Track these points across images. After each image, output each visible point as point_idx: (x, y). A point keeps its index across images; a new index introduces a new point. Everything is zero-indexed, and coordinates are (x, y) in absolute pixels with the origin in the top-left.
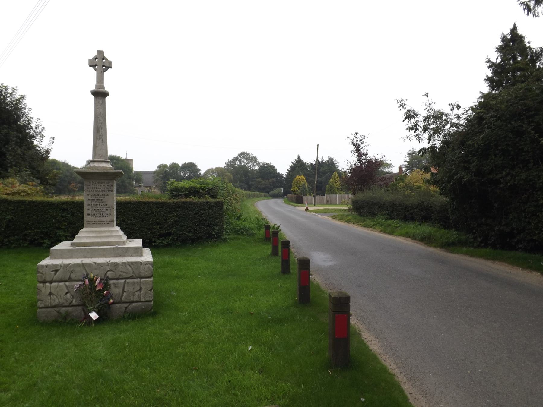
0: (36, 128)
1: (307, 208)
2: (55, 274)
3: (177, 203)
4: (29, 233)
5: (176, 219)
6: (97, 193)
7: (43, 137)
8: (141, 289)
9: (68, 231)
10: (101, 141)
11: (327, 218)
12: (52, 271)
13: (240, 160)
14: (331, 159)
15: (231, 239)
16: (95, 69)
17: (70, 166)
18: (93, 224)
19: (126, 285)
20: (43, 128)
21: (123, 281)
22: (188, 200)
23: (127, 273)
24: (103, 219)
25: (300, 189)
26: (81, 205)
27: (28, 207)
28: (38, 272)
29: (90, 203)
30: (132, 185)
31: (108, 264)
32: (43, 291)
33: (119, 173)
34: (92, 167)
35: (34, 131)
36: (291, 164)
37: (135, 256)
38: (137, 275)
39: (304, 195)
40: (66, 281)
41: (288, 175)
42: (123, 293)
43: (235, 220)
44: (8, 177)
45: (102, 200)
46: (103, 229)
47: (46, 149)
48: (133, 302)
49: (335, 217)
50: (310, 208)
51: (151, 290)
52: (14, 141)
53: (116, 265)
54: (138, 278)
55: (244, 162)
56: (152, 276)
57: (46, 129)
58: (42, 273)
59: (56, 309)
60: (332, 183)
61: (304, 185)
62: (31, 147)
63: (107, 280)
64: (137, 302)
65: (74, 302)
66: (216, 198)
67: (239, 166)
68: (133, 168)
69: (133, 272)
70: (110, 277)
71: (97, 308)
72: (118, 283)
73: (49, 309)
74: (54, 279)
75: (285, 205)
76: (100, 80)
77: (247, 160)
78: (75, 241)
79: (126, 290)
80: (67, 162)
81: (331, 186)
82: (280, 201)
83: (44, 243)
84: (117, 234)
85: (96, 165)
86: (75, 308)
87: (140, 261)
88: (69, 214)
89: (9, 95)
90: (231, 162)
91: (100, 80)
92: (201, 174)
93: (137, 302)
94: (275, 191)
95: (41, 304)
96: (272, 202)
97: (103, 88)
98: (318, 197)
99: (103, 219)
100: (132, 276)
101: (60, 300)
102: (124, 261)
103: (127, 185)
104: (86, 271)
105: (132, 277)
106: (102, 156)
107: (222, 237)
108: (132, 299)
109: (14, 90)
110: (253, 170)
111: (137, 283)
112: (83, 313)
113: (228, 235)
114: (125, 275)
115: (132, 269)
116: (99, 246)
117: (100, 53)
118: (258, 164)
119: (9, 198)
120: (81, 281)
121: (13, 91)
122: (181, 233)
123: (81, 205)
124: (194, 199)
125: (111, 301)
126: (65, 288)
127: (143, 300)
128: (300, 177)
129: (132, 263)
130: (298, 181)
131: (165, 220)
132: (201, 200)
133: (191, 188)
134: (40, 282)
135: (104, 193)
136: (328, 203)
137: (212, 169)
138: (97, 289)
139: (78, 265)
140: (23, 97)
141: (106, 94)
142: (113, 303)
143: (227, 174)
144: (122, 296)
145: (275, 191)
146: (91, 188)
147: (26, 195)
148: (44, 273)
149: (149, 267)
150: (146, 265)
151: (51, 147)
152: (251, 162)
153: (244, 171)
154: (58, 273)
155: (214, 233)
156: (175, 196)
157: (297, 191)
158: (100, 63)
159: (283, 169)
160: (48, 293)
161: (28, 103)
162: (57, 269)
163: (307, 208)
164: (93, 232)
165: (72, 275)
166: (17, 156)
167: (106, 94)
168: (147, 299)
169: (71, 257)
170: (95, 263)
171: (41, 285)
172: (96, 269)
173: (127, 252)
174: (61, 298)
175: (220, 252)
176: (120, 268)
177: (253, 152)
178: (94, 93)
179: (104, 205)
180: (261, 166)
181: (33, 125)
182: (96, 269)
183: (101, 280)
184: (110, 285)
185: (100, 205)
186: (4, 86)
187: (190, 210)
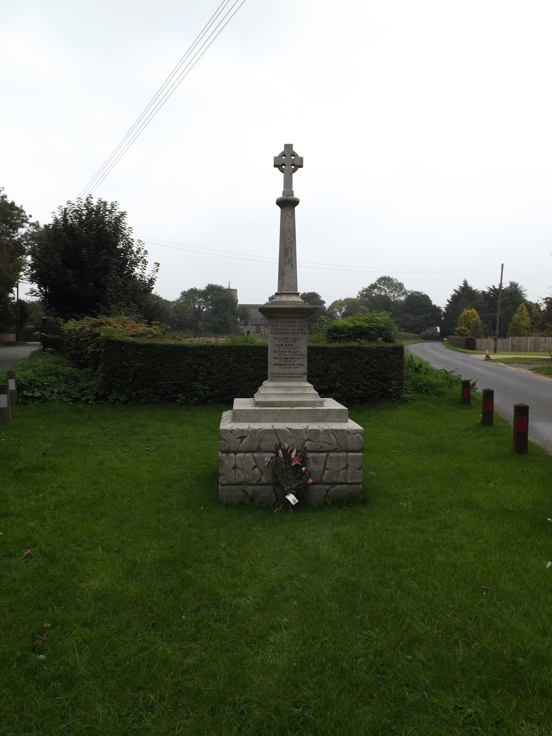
0: (137, 252)
1: (487, 356)
2: (241, 442)
3: (342, 348)
4: (161, 385)
5: (340, 370)
6: (286, 336)
7: (145, 262)
8: (346, 467)
9: (206, 383)
10: (290, 266)
11: (523, 371)
12: (238, 438)
13: (380, 289)
14: (514, 286)
15: (412, 399)
16: (282, 171)
17: (161, 298)
18: (279, 377)
19: (328, 460)
20: (146, 251)
21: (325, 454)
22: (355, 344)
23: (330, 444)
24: (294, 371)
25: (469, 328)
26: (263, 350)
27: (160, 352)
28: (221, 439)
29: (277, 349)
30: (237, 323)
31: (306, 431)
33: (310, 309)
34: (280, 302)
35: (135, 256)
36: (453, 293)
37: (338, 422)
38: (343, 448)
39: (477, 338)
40: (253, 452)
41: (448, 308)
42: (324, 471)
43: (413, 373)
44: (109, 315)
45: (292, 345)
46: (293, 384)
47: (150, 277)
48: (334, 484)
49: (537, 371)
50: (492, 357)
51: (360, 469)
52: (114, 269)
53: (316, 432)
54: (343, 451)
55: (386, 291)
56: (362, 449)
57: (149, 252)
58: (225, 440)
59: (240, 487)
60: (519, 321)
61: (477, 322)
62: (131, 278)
63: (304, 453)
64: (341, 483)
65: (263, 480)
66: (390, 341)
67: (379, 295)
68: (237, 301)
69: (338, 444)
70: (308, 448)
71: (295, 489)
72: (318, 457)
73: (233, 487)
74: (240, 449)
75: (447, 351)
76: (288, 183)
77: (389, 288)
78: (258, 398)
79: (328, 467)
80: (157, 294)
81: (516, 325)
82: (438, 345)
83: (178, 398)
84: (307, 392)
85: (284, 298)
86: (264, 487)
87: (346, 428)
88: (208, 362)
89: (107, 213)
90: (366, 290)
91: (288, 183)
92: (325, 308)
93: (341, 483)
94: (429, 331)
95: (223, 479)
96: (427, 346)
97: (292, 193)
98: (499, 341)
99: (294, 371)
100: (336, 449)
101: (247, 476)
102: (327, 428)
103: (231, 323)
104: (279, 440)
105: (335, 451)
106: (291, 287)
107: (401, 396)
108: (335, 480)
109: (113, 206)
110: (397, 301)
111: (343, 458)
112: (274, 495)
113: (408, 393)
115: (337, 439)
116: (286, 407)
117: (289, 147)
118: (405, 293)
119: (137, 340)
120: (273, 452)
121: (113, 207)
122: (347, 389)
123: (263, 350)
124: (365, 343)
125: (310, 481)
126: (252, 460)
127: (349, 481)
128: (469, 311)
129: (337, 431)
130: (466, 317)
131: (327, 371)
132: (373, 345)
133: (356, 328)
134: (223, 452)
135: (295, 336)
136: (514, 348)
137: (341, 300)
138: (293, 465)
139: (269, 431)
140: (123, 214)
141: (296, 202)
142: (312, 484)
143: (361, 307)
144: (323, 474)
145: (429, 331)
146: (278, 329)
147: (152, 337)
148: (228, 440)
149: (358, 437)
150: (354, 434)
151: (156, 275)
152: (395, 290)
153: (383, 303)
154: (244, 441)
155: (390, 390)
156: (335, 339)
157: (465, 331)
158: (288, 162)
159: (441, 300)
160: (232, 466)
161: (128, 222)
162: (244, 435)
163: (487, 356)
164: (281, 387)
165: (261, 444)
166: (119, 288)
167: (296, 202)
168: (355, 481)
169: (258, 421)
170: (290, 429)
171: (224, 455)
172: (291, 437)
173: (327, 415)
174: (248, 474)
175: (402, 415)
177: (398, 277)
178: (280, 203)
179: (294, 352)
180: (409, 296)
181: (135, 249)
182: (291, 437)
183: (297, 452)
184: (308, 459)
185: (289, 352)
186: (102, 202)
187: (359, 359)
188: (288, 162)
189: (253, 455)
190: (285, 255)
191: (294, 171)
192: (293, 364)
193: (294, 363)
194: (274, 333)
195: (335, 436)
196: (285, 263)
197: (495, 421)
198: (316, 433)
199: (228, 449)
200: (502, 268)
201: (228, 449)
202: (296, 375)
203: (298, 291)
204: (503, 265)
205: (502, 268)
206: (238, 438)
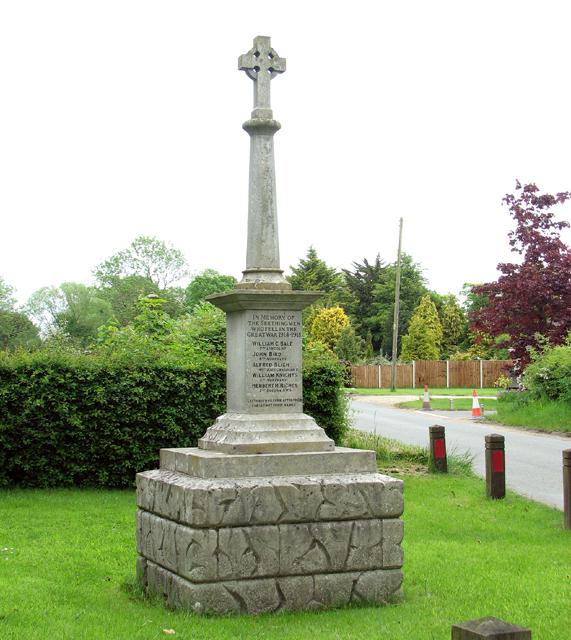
2: (226, 510)
6: (271, 340)
12: (221, 504)
21: (351, 523)
24: (282, 395)
32: (204, 545)
42: (349, 550)
58: (202, 509)
59: (226, 584)
72: (340, 529)
76: (261, 98)
86: (261, 581)
91: (261, 98)
93: (374, 569)
99: (282, 395)
114: (353, 512)
146: (258, 329)
154: (231, 507)
170: (299, 486)
176: (270, 499)
188: (262, 63)
189: (244, 531)
190: (263, 211)
191: (272, 77)
192: (282, 385)
193: (283, 383)
194: (252, 335)
195: (363, 493)
196: (263, 224)
197: (507, 493)
198: (337, 490)
199: (207, 521)
200: (401, 226)
201: (207, 521)
202: (286, 402)
203: (281, 269)
204: (401, 220)
205: (401, 226)
206: (221, 504)
